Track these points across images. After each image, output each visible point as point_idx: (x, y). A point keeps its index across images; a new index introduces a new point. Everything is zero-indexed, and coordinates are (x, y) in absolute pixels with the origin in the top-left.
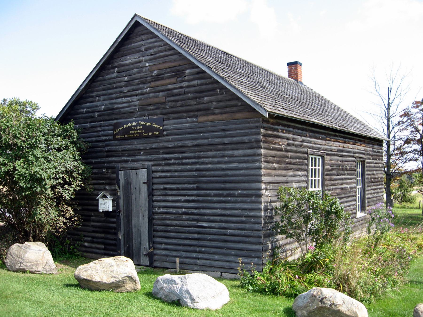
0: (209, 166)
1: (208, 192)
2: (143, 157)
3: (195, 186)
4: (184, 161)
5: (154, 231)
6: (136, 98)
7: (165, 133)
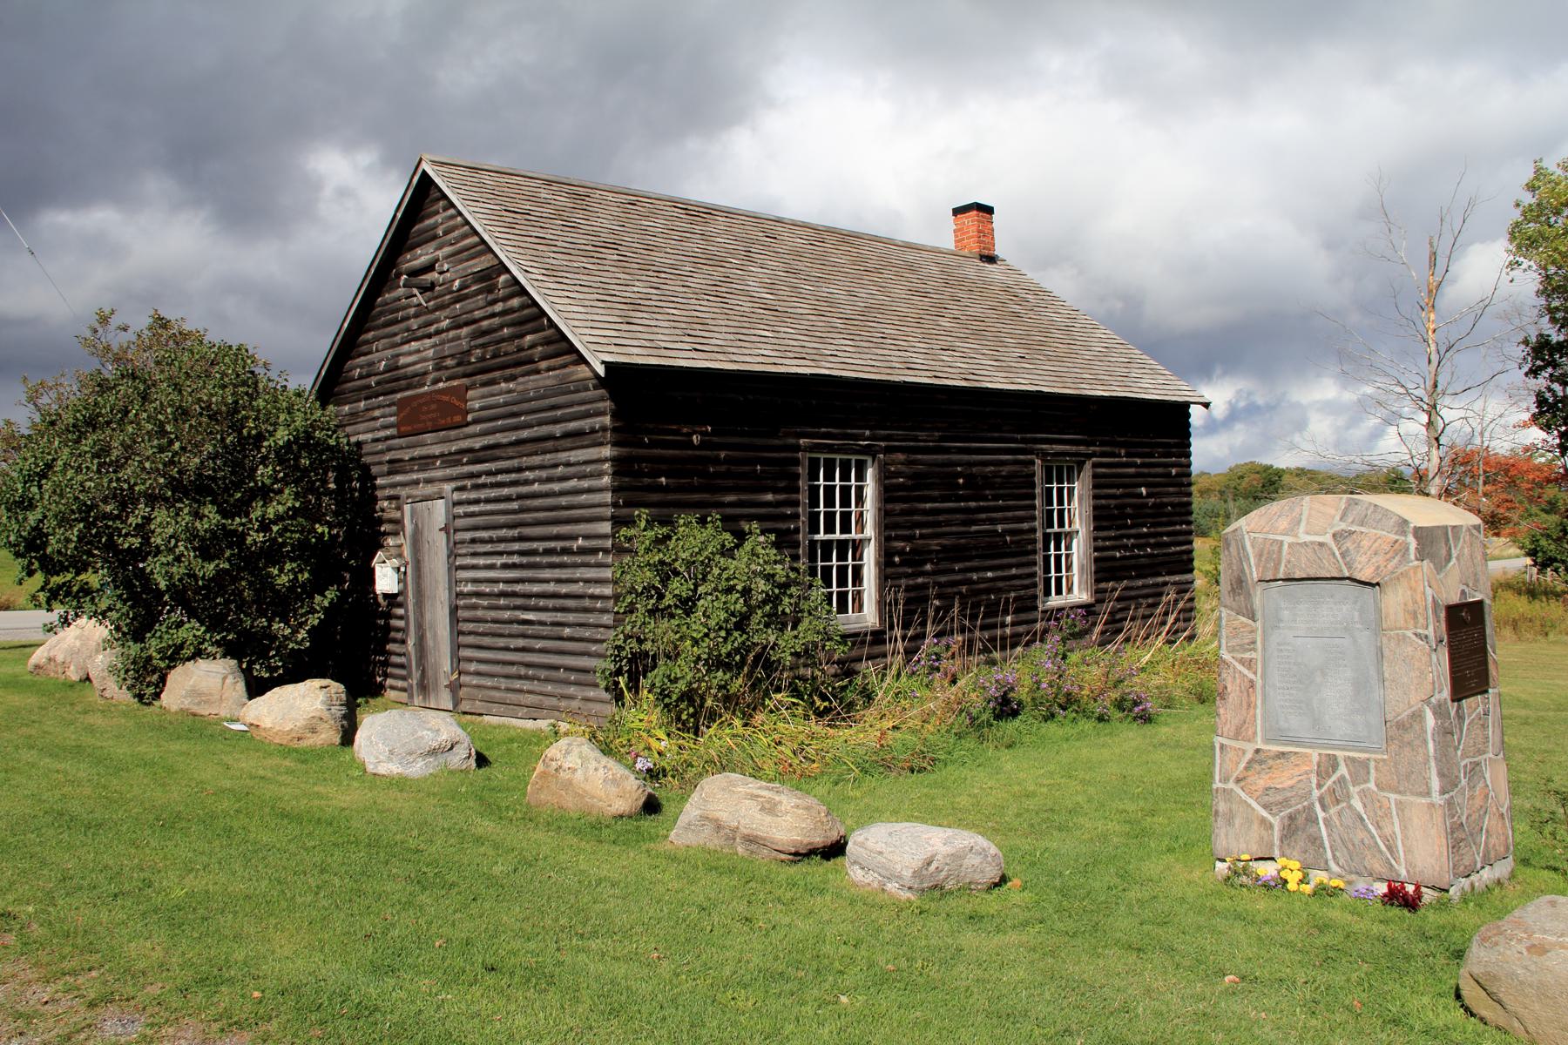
0: (1014, 571)
1: (535, 545)
2: (439, 473)
3: (515, 532)
4: (500, 478)
5: (461, 633)
6: (428, 342)
7: (469, 418)
